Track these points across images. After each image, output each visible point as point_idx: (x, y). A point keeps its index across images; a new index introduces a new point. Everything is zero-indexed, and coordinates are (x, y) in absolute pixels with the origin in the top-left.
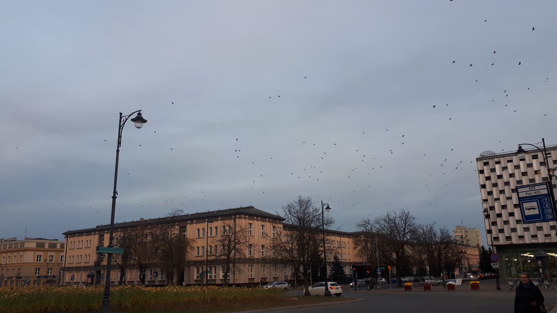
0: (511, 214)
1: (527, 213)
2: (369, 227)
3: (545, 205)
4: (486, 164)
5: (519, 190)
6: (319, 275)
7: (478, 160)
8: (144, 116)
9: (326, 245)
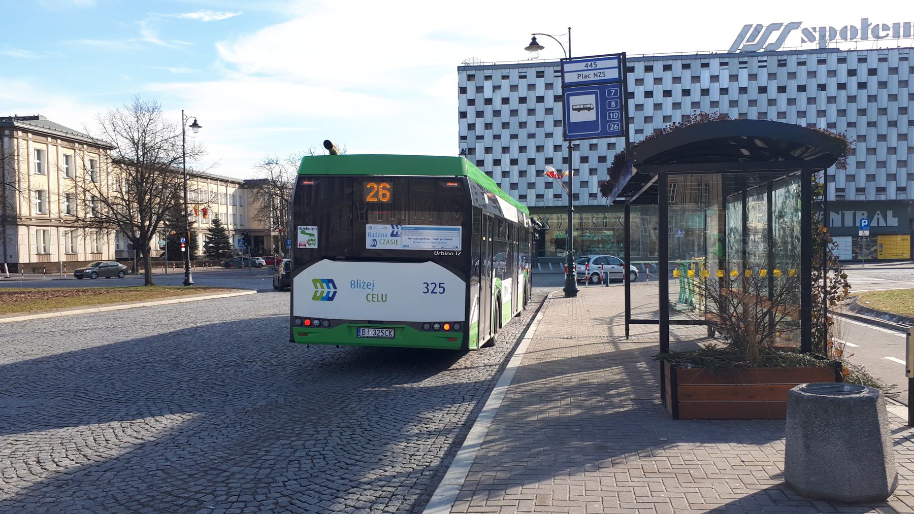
0: (549, 111)
1: (575, 117)
2: (276, 170)
3: (610, 103)
4: (470, 78)
5: (567, 67)
6: (183, 250)
7: (460, 69)
8: (199, 123)
9: (189, 196)
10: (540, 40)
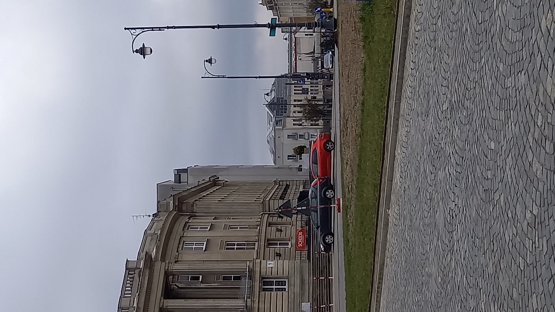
10: (138, 46)
